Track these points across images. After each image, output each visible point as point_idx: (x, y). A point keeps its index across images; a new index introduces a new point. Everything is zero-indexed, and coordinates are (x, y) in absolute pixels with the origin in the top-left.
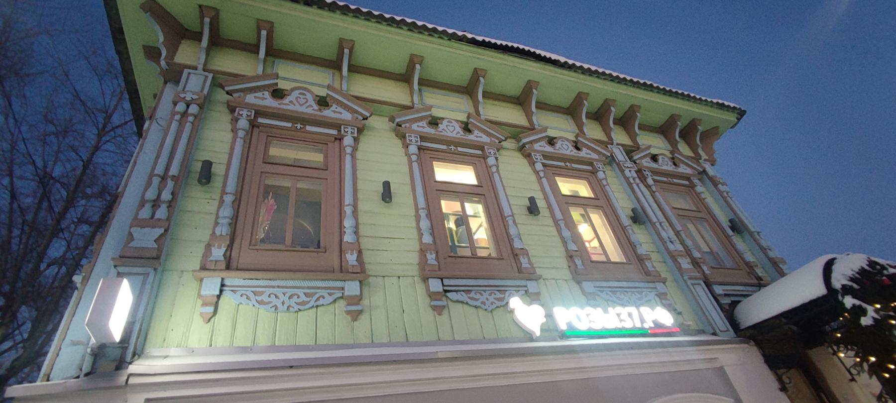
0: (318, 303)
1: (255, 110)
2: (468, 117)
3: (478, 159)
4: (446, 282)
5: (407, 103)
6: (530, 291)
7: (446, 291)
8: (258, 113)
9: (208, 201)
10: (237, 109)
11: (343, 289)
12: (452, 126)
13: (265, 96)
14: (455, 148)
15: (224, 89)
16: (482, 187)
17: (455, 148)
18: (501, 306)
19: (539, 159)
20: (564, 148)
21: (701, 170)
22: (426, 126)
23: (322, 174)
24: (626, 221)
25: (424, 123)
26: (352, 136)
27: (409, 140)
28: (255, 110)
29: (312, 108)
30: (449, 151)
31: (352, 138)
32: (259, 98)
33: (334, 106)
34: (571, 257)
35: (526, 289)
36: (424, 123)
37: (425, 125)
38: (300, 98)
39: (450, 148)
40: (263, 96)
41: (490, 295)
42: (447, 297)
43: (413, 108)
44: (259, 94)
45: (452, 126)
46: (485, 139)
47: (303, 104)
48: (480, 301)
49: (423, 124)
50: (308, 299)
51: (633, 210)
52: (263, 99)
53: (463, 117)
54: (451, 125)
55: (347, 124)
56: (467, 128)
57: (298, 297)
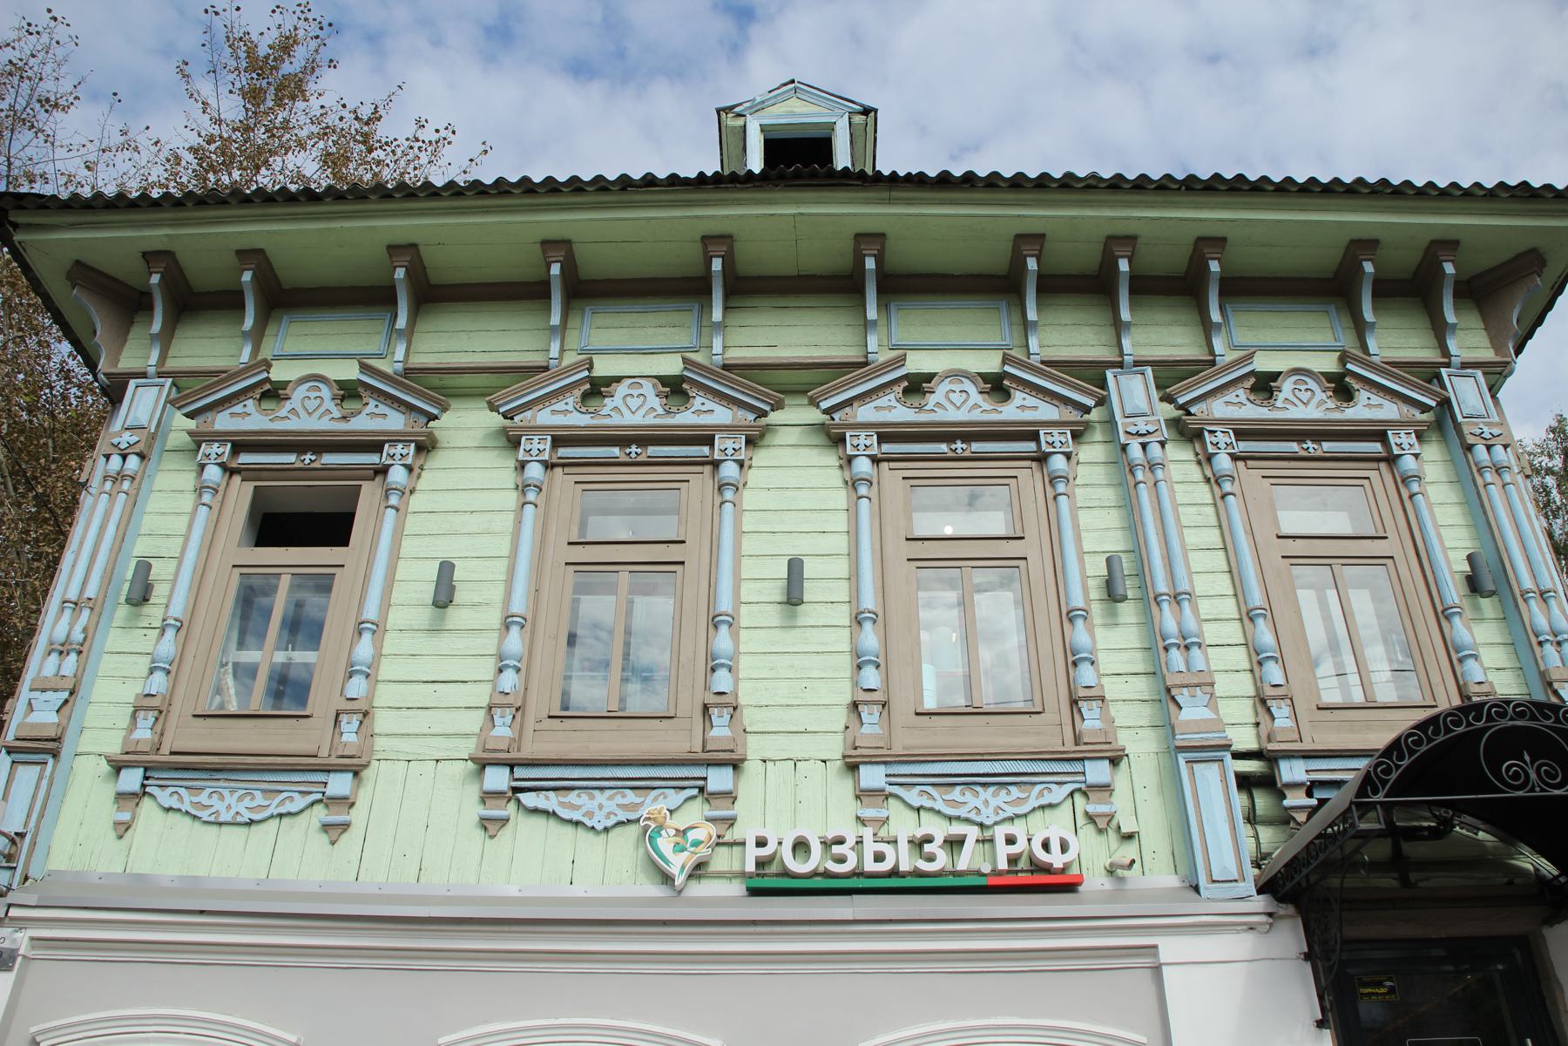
0: (283, 810)
1: (552, 436)
2: (1344, 358)
3: (1374, 465)
4: (519, 773)
5: (850, 354)
6: (712, 786)
7: (516, 790)
8: (239, 447)
9: (145, 631)
10: (387, 446)
11: (705, 779)
12: (1307, 390)
13: (247, 410)
14: (1316, 447)
15: (818, 406)
16: (1386, 538)
17: (1316, 447)
18: (1018, 816)
19: (1057, 444)
20: (952, 402)
21: (174, 388)
22: (1245, 402)
23: (672, 553)
24: (1454, 592)
25: (1241, 394)
26: (1229, 454)
27: (1047, 442)
28: (552, 436)
29: (655, 413)
30: (1304, 454)
31: (1227, 456)
32: (883, 408)
33: (699, 400)
34: (1263, 702)
35: (701, 783)
36: (1241, 394)
37: (894, 403)
38: (309, 398)
39: (1305, 446)
40: (245, 410)
41: (240, 799)
42: (519, 801)
43: (866, 364)
44: (238, 409)
45: (1307, 390)
46: (1389, 410)
47: (1309, 401)
48: (584, 810)
49: (890, 400)
50: (266, 803)
51: (1470, 558)
52: (890, 408)
53: (1327, 363)
54: (1303, 387)
55: (396, 438)
56: (1341, 388)
57: (252, 799)
